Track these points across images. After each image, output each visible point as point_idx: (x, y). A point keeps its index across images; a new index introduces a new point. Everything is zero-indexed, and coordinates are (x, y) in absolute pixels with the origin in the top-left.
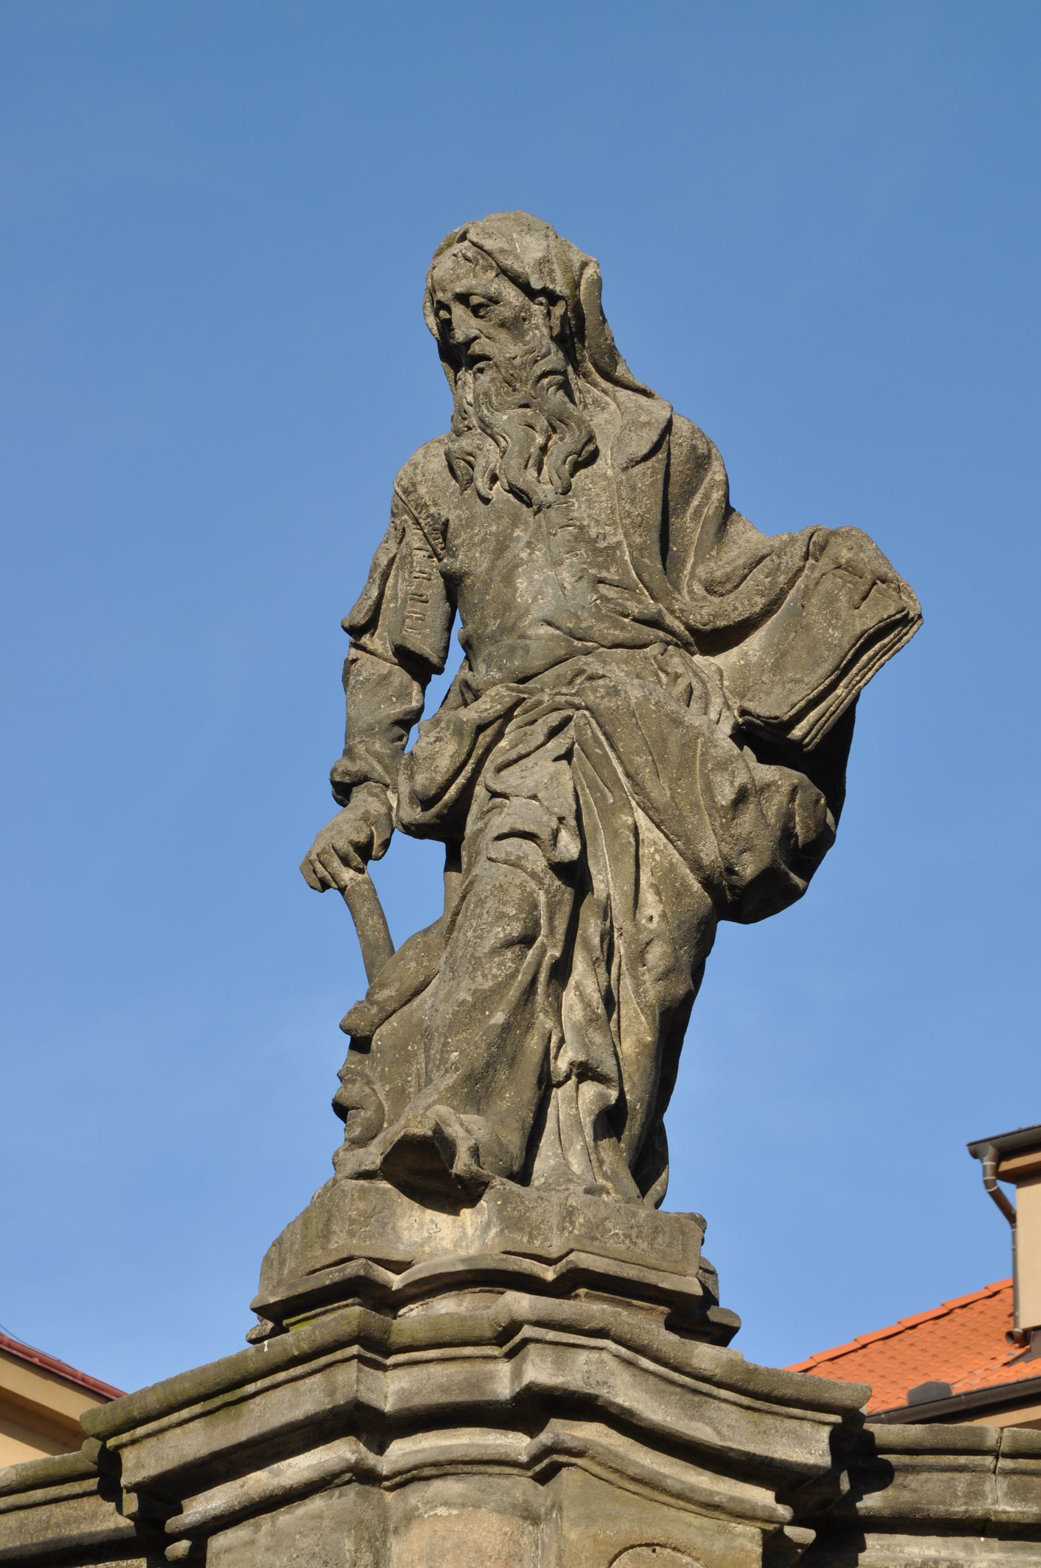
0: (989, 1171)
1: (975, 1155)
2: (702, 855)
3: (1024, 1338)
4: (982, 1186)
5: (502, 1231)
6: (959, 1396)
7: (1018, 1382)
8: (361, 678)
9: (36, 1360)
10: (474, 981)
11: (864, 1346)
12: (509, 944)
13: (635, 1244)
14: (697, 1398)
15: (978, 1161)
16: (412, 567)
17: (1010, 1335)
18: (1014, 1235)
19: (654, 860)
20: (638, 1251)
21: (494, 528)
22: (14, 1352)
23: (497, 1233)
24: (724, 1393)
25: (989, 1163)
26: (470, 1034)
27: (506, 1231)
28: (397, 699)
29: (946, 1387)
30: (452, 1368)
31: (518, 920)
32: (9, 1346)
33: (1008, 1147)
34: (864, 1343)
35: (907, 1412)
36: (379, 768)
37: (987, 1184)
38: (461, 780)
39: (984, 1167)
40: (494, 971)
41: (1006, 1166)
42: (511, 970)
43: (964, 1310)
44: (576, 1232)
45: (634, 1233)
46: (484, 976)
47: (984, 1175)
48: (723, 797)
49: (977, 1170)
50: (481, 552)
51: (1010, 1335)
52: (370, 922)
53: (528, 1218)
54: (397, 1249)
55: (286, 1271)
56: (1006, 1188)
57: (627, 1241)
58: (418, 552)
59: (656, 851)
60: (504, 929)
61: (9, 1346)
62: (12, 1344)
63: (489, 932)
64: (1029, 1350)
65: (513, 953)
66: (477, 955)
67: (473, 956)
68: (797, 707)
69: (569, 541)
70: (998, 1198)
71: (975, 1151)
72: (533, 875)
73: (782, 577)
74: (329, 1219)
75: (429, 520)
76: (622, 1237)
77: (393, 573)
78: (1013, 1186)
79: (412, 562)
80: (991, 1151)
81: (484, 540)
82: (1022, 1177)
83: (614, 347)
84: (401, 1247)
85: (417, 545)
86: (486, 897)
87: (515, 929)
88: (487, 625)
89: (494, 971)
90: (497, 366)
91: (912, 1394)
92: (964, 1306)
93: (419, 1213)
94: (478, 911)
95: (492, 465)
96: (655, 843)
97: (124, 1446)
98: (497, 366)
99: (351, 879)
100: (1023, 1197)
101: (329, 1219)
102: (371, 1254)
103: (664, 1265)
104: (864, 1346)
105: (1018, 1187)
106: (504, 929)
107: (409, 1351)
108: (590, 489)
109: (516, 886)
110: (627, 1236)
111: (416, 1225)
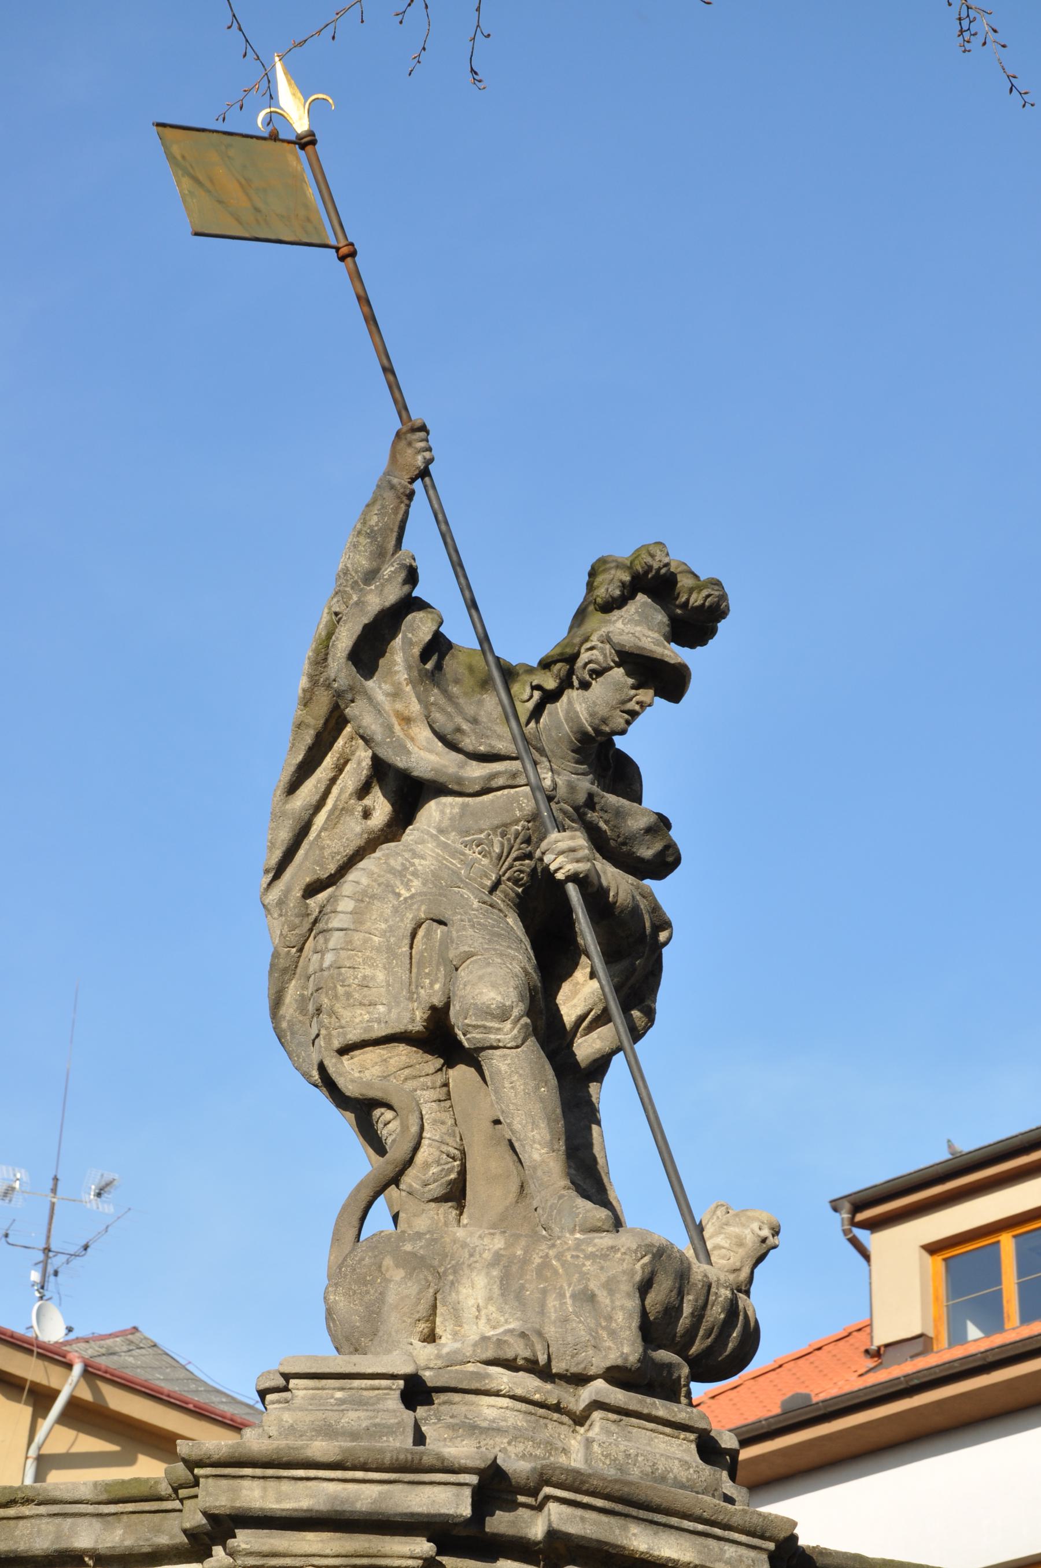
0: (846, 1222)
1: (836, 1209)
3: (876, 1354)
4: (841, 1234)
6: (817, 1403)
7: (860, 1390)
9: (191, 1406)
11: (780, 1366)
15: (837, 1214)
17: (867, 1352)
18: (870, 1271)
22: (172, 1400)
25: (846, 1216)
29: (808, 1397)
32: (169, 1396)
33: (859, 1203)
34: (780, 1363)
35: (781, 1418)
37: (845, 1232)
39: (843, 1219)
41: (860, 1217)
43: (860, 1333)
47: (843, 1225)
49: (837, 1221)
51: (867, 1352)
56: (861, 1234)
61: (169, 1396)
62: (172, 1394)
64: (881, 1363)
70: (855, 1242)
71: (835, 1206)
78: (867, 1232)
80: (847, 1206)
82: (875, 1225)
83: (330, 1277)
91: (784, 1403)
92: (859, 1330)
97: (498, 695)
100: (874, 1241)
104: (780, 1366)
105: (872, 1233)
107: (658, 1424)
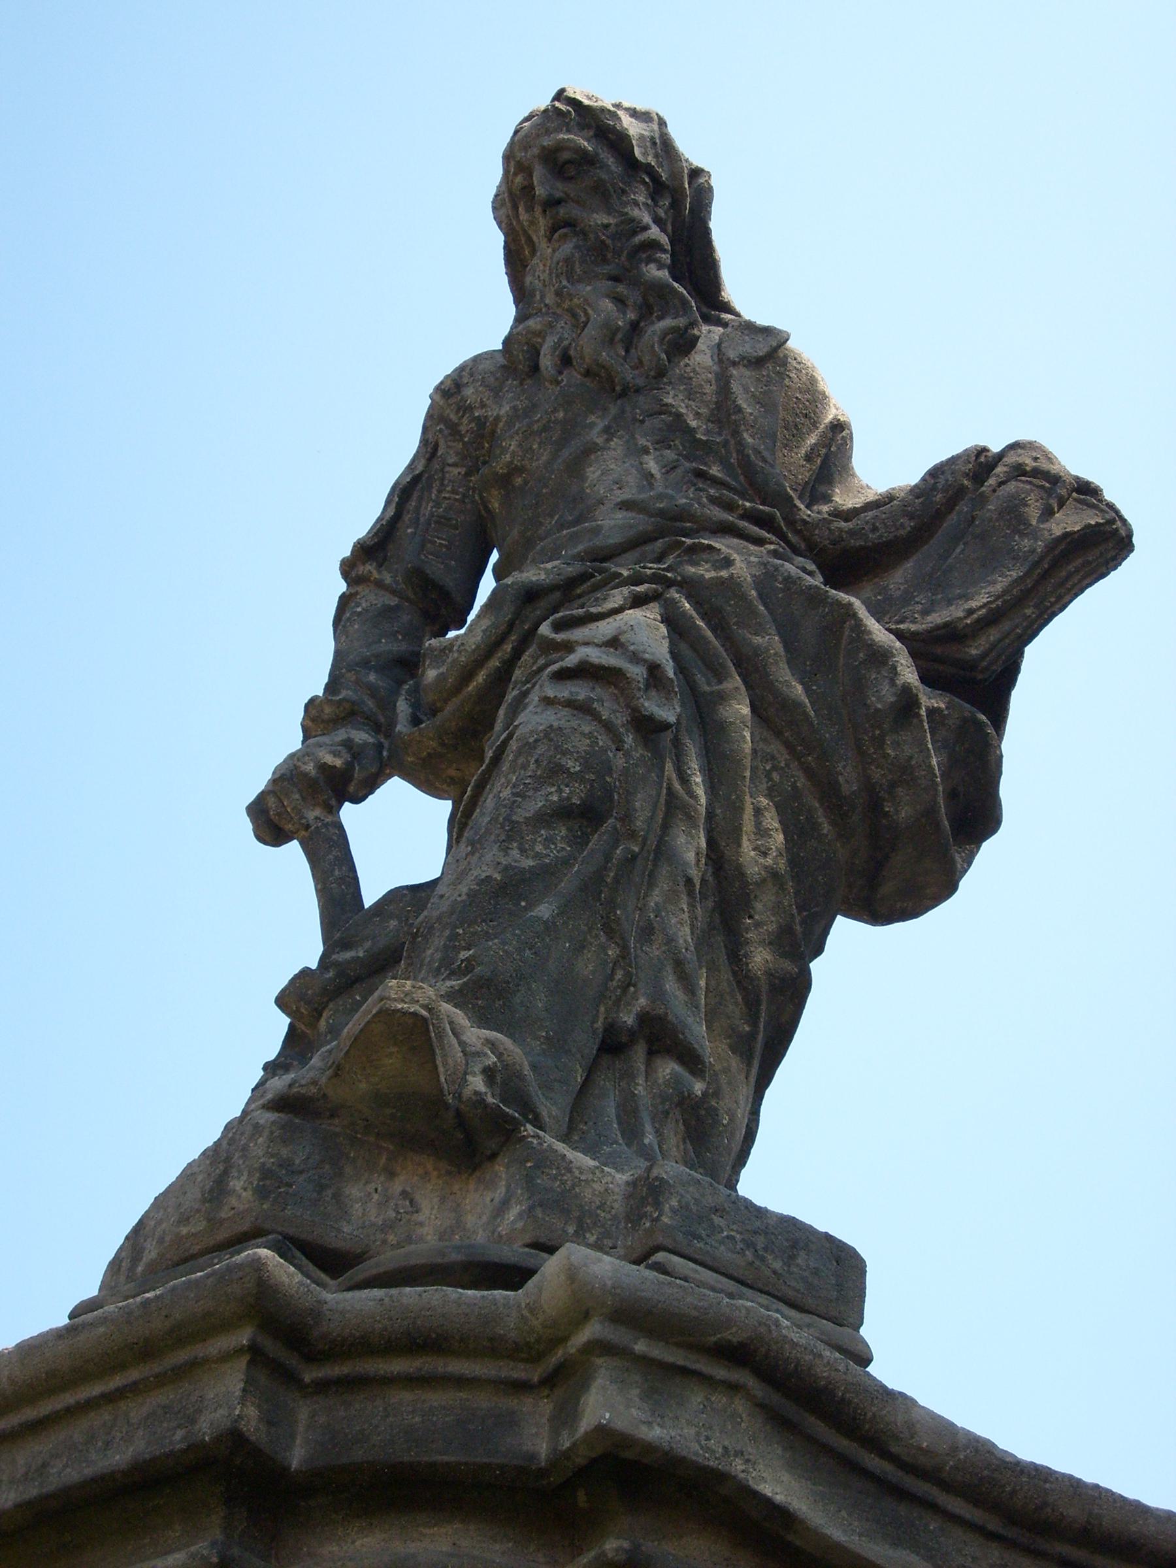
2: (841, 779)
5: (531, 1209)
8: (359, 609)
10: (506, 854)
12: (563, 812)
13: (763, 1259)
14: (903, 1510)
16: (442, 484)
19: (771, 779)
20: (768, 1273)
21: (561, 415)
23: (520, 1215)
24: (956, 1505)
26: (494, 927)
27: (539, 1212)
28: (404, 637)
30: (436, 1398)
31: (582, 780)
36: (371, 703)
38: (495, 663)
40: (539, 848)
42: (564, 853)
44: (665, 1219)
45: (761, 1241)
46: (523, 851)
48: (879, 699)
50: (540, 444)
52: (337, 873)
53: (577, 1196)
54: (339, 1230)
55: (140, 1269)
57: (749, 1254)
58: (451, 469)
59: (774, 768)
60: (560, 791)
63: (536, 790)
65: (570, 830)
66: (514, 818)
67: (507, 819)
68: (975, 616)
69: (660, 429)
72: (608, 727)
73: (940, 496)
74: (226, 1173)
75: (473, 425)
76: (740, 1246)
77: (416, 495)
79: (443, 479)
81: (545, 429)
84: (347, 1229)
85: (451, 461)
86: (536, 741)
87: (575, 793)
88: (541, 524)
89: (539, 848)
90: (585, 234)
93: (382, 1178)
94: (521, 760)
95: (566, 343)
96: (773, 758)
98: (585, 234)
99: (317, 818)
101: (226, 1173)
102: (291, 1231)
103: (810, 1302)
106: (560, 791)
108: (691, 378)
109: (583, 734)
110: (750, 1245)
111: (376, 1197)
